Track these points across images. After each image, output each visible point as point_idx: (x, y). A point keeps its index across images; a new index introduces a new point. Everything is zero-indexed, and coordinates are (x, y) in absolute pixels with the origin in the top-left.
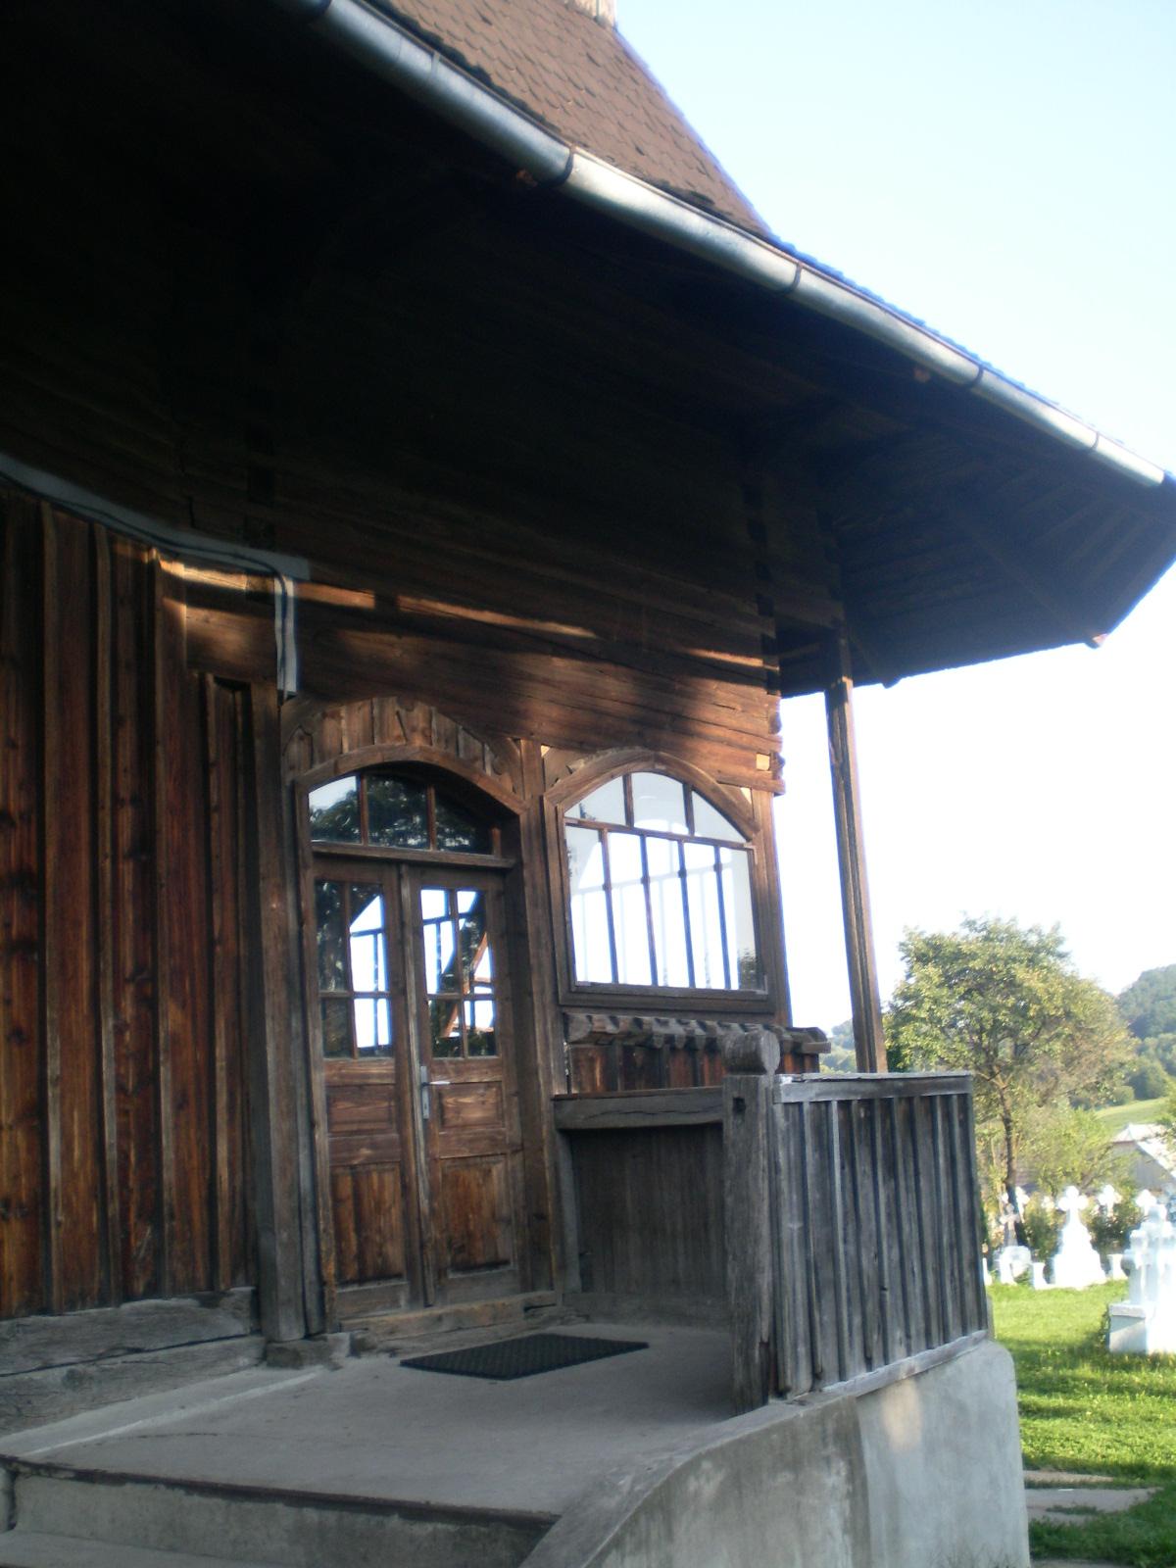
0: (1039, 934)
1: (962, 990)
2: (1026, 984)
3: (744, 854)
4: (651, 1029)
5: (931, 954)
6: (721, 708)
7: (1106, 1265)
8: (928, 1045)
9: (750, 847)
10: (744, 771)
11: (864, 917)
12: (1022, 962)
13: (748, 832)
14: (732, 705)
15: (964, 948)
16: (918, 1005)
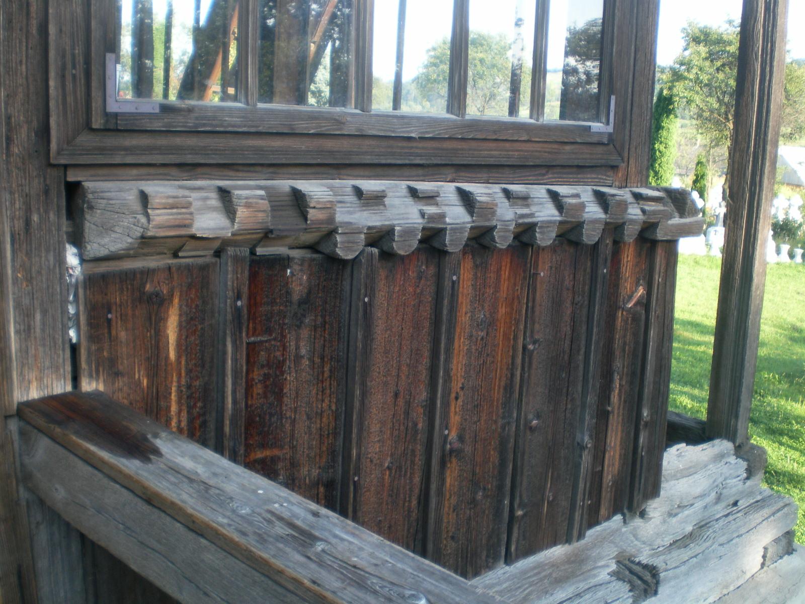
1: (719, 64)
4: (331, 219)
5: (702, 38)
11: (780, 9)
15: (725, 37)
16: (688, 70)
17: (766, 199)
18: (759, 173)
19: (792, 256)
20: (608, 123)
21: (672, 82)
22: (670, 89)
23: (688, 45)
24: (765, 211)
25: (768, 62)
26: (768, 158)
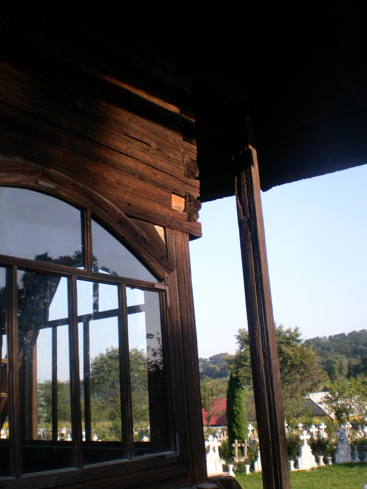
0: (290, 333)
2: (286, 352)
3: (156, 295)
6: (132, 140)
7: (317, 461)
8: (249, 376)
9: (163, 287)
10: (157, 207)
12: (284, 344)
13: (160, 271)
14: (147, 140)
17: (284, 468)
18: (277, 453)
19: (325, 461)
20: (176, 450)
21: (237, 368)
22: (236, 373)
23: (243, 346)
24: (285, 475)
25: (270, 387)
26: (280, 443)
